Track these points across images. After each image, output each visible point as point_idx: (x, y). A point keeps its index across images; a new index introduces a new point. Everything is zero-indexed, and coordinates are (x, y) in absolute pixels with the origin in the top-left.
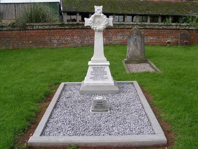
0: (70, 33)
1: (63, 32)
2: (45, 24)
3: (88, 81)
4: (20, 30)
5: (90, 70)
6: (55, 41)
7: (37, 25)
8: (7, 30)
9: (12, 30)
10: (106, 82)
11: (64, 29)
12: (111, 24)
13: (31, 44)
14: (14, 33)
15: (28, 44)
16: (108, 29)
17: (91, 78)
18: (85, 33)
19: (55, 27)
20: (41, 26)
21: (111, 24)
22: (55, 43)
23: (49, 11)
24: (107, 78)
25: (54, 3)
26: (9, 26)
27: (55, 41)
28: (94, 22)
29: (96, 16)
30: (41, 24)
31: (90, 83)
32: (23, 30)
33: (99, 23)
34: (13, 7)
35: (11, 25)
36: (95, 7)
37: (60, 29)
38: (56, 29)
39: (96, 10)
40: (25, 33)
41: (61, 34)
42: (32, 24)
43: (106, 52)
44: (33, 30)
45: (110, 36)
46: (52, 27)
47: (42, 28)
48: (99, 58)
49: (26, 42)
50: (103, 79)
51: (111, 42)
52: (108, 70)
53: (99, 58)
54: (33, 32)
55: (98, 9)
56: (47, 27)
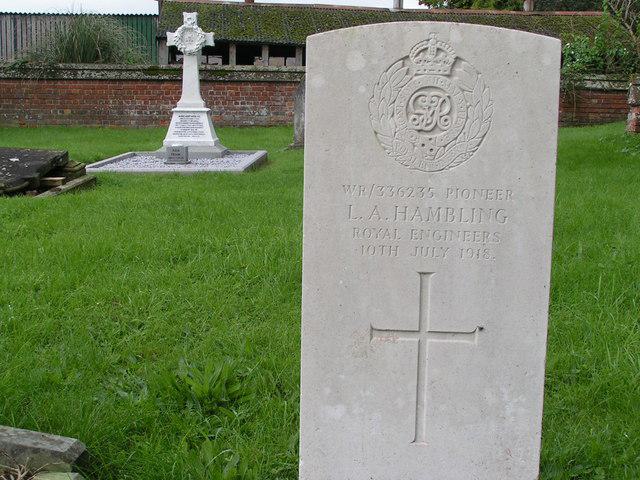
0: (173, 93)
1: (154, 88)
2: (107, 66)
3: (173, 138)
4: (41, 80)
5: (175, 119)
6: (133, 113)
7: (86, 70)
8: (8, 79)
9: (20, 79)
10: (201, 139)
11: (158, 81)
12: (211, 43)
13: (69, 117)
14: (24, 86)
15: (61, 117)
16: (206, 51)
17: (175, 133)
18: (212, 93)
19: (134, 76)
20: (98, 71)
21: (211, 43)
22: (133, 118)
23: (120, 32)
24: (202, 133)
25: (149, 19)
26: (13, 68)
27: (133, 113)
28: (181, 38)
29: (185, 29)
30: (97, 66)
31: (173, 142)
32: (48, 80)
33: (191, 41)
34: (8, 24)
35: (17, 66)
36: (184, 13)
37: (147, 80)
38: (137, 80)
39: (185, 19)
40: (54, 87)
41: (149, 93)
42: (74, 65)
43: (204, 94)
44: (75, 80)
45: (279, 104)
46: (125, 75)
47: (98, 76)
48: (191, 95)
49: (55, 112)
50: (196, 134)
51: (281, 118)
52: (205, 120)
53: (191, 95)
54: (75, 88)
55: (189, 18)
56: (112, 75)
